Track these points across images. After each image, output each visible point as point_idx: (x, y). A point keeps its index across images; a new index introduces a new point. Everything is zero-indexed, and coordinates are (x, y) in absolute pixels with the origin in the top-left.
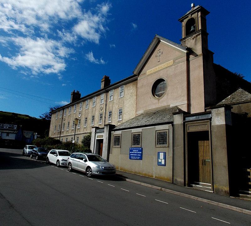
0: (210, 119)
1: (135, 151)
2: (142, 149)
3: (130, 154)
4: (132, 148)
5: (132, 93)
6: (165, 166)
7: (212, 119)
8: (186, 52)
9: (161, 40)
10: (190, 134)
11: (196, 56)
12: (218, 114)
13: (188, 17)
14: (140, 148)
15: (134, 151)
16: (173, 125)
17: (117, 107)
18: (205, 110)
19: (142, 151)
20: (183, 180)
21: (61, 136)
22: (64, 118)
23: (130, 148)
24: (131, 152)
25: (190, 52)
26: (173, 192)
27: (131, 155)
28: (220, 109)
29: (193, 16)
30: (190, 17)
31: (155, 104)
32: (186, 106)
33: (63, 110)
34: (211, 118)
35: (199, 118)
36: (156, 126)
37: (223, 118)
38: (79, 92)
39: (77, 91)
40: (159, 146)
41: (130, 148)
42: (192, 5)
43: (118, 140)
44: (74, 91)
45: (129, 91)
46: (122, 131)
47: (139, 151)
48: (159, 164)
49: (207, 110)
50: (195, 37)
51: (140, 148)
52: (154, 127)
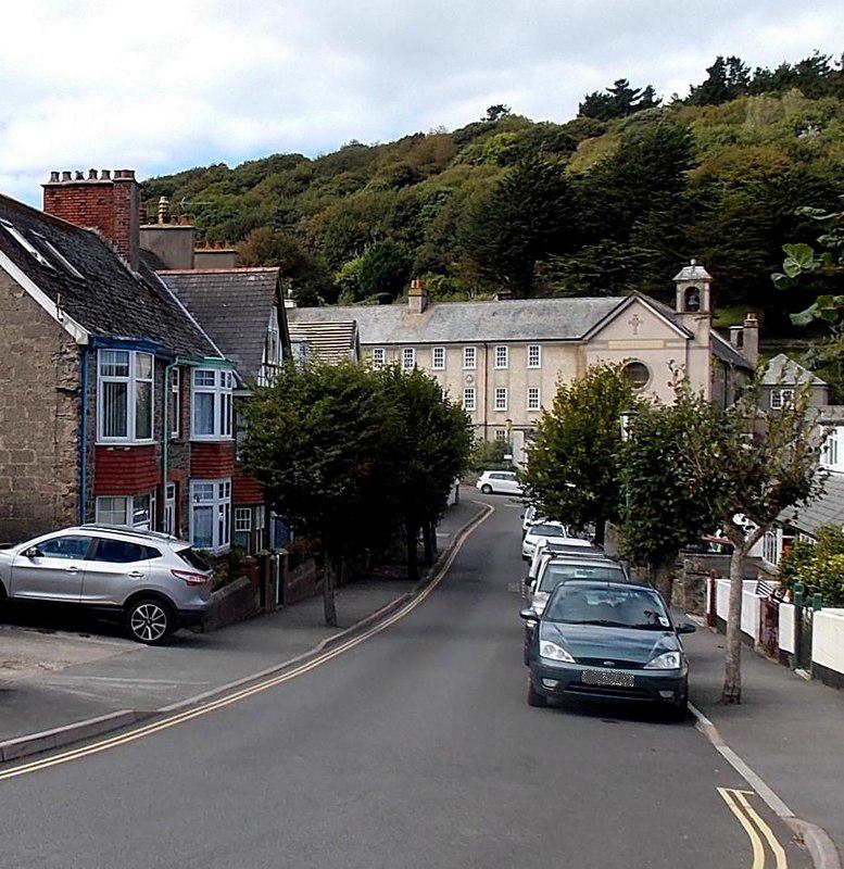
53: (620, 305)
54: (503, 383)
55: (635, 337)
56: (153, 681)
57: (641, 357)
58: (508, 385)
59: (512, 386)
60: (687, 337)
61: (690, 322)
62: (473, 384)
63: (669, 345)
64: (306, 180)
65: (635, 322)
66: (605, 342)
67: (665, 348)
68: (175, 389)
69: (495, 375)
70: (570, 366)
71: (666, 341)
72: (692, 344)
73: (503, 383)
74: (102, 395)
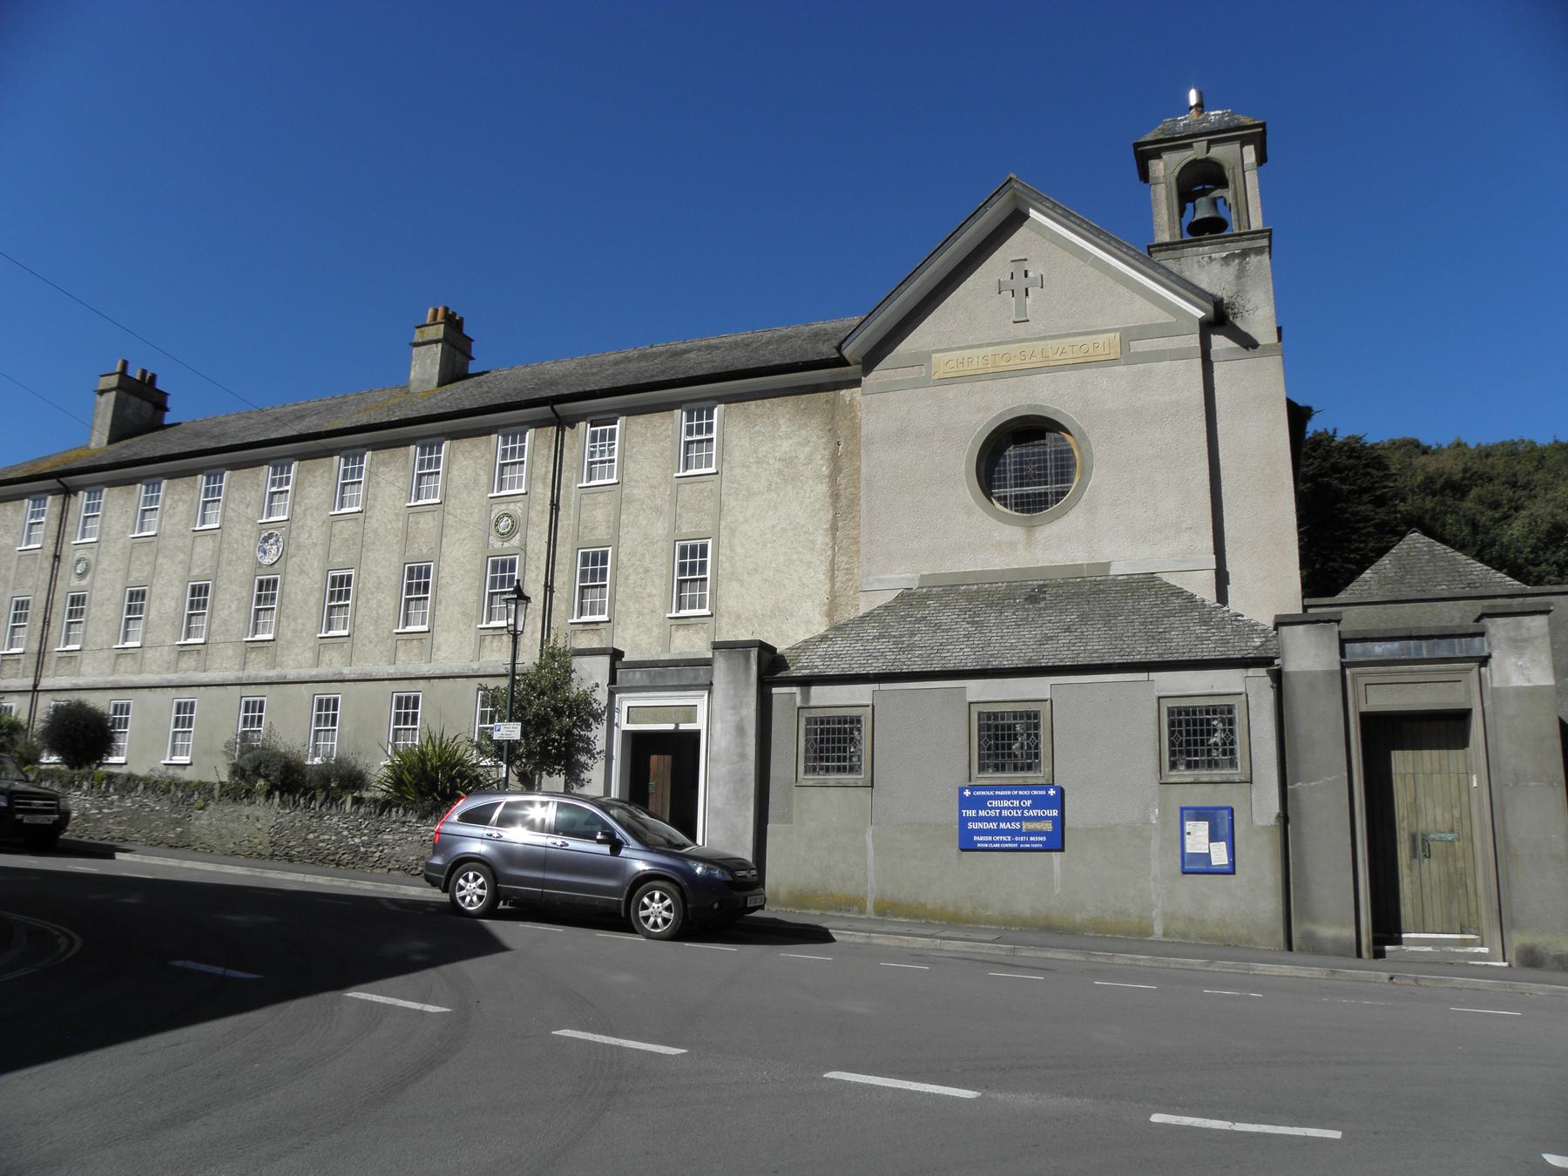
0: (1484, 661)
1: (1006, 803)
2: (1061, 792)
3: (964, 821)
4: (973, 788)
5: (789, 461)
6: (1233, 872)
7: (1493, 662)
8: (1200, 314)
9: (1033, 213)
10: (1367, 719)
11: (1246, 348)
12: (1518, 644)
13: (1189, 146)
14: (1046, 787)
15: (995, 803)
16: (1278, 677)
17: (660, 528)
18: (1305, 608)
19: (1060, 801)
20: (1350, 933)
21: (45, 683)
22: (70, 554)
23: (962, 790)
24: (971, 813)
25: (1219, 319)
26: (318, 859)
27: (971, 826)
28: (1527, 620)
29: (1217, 152)
30: (1198, 151)
31: (998, 545)
32: (1209, 577)
33: (68, 492)
34: (1489, 656)
35: (1419, 649)
36: (1154, 675)
37: (1545, 659)
38: (153, 377)
39: (144, 372)
40: (1182, 774)
41: (962, 790)
42: (1193, 98)
43: (834, 744)
44: (125, 364)
45: (765, 448)
46: (875, 686)
47: (1039, 803)
48: (1197, 866)
49: (1311, 611)
50: (1233, 256)
51: (1046, 787)
52: (1142, 676)
58: (616, 541)
62: (516, 541)
66: (922, 359)
67: (1127, 357)
70: (810, 459)
71: (1129, 335)
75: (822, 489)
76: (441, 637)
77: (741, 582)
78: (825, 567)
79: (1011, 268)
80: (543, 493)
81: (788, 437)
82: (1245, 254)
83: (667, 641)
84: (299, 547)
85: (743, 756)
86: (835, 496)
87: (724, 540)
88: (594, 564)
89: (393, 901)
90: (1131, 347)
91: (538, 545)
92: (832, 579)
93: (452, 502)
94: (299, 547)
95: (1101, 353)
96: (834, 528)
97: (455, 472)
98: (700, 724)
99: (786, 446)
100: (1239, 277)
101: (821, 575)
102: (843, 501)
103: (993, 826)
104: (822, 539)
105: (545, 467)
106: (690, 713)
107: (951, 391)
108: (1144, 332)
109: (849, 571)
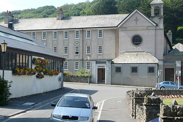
5: (111, 37)
16: (158, 65)
39: (8, 11)
53: (127, 17)
54: (89, 44)
55: (137, 25)
56: (30, 108)
57: (129, 40)
58: (91, 45)
59: (92, 45)
60: (155, 25)
61: (156, 20)
62: (78, 44)
63: (149, 28)
64: (54, 11)
65: (137, 20)
66: (126, 28)
67: (147, 29)
68: (61, 64)
69: (86, 41)
70: (113, 37)
71: (148, 27)
72: (157, 28)
73: (89, 44)
74: (26, 60)
75: (115, 41)
76: (70, 55)
77: (106, 51)
78: (115, 49)
79: (136, 18)
80: (81, 39)
81: (111, 34)
82: (160, 18)
83: (97, 57)
84: (48, 43)
85: (110, 71)
86: (116, 42)
87: (104, 46)
88: (89, 48)
89: (100, 84)
90: (148, 28)
91: (81, 45)
92: (116, 51)
93: (70, 39)
94: (48, 43)
95: (145, 29)
96: (116, 45)
97: (70, 35)
98: (105, 68)
99: (110, 36)
100: (160, 21)
101: (114, 50)
102: (117, 42)
103: (52, 64)
104: (114, 46)
105: (81, 36)
106: (104, 67)
107: (128, 32)
108: (149, 27)
109: (118, 50)
